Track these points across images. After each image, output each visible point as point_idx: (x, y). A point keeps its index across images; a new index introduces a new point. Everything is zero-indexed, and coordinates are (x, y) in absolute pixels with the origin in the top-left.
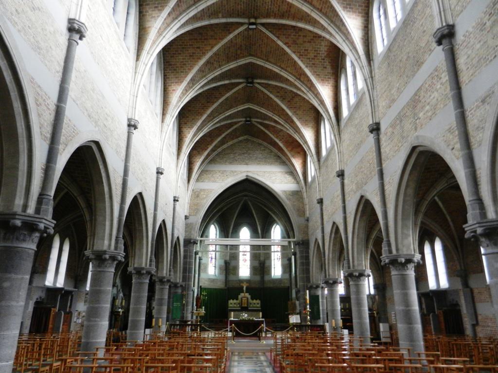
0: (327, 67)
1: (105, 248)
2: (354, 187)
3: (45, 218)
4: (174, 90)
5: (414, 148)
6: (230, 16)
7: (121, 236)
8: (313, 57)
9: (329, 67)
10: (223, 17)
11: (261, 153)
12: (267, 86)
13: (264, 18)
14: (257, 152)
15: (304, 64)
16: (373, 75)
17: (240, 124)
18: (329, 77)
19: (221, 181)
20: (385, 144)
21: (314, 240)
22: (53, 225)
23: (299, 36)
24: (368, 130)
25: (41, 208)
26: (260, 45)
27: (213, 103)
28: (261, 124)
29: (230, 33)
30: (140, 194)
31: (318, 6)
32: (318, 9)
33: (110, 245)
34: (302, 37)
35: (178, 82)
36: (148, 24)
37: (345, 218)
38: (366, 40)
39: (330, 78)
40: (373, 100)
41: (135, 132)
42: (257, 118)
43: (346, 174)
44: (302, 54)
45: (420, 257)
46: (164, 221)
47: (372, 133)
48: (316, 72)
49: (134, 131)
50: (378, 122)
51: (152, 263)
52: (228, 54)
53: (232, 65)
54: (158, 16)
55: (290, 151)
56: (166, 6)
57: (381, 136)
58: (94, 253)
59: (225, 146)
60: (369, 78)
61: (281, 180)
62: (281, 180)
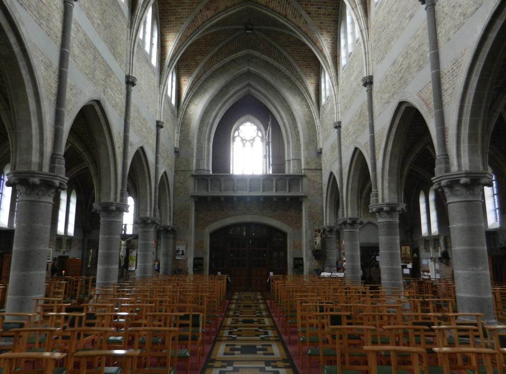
3: (60, 176)
5: (401, 104)
7: (126, 190)
16: (369, 26)
22: (66, 181)
24: (362, 83)
30: (142, 148)
33: (151, 214)
37: (373, 139)
38: (334, 49)
41: (133, 89)
43: (343, 125)
45: (405, 206)
46: (165, 173)
47: (365, 86)
49: (133, 88)
51: (157, 213)
58: (100, 204)
60: (365, 29)
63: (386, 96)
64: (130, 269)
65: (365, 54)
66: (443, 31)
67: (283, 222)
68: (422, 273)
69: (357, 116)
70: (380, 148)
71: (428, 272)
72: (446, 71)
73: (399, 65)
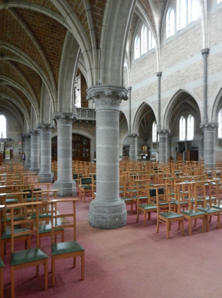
63: (171, 84)
64: (6, 158)
65: (159, 61)
66: (211, 69)
67: (90, 134)
68: (151, 158)
69: (147, 87)
70: (164, 106)
71: (155, 157)
72: (210, 85)
73: (182, 74)
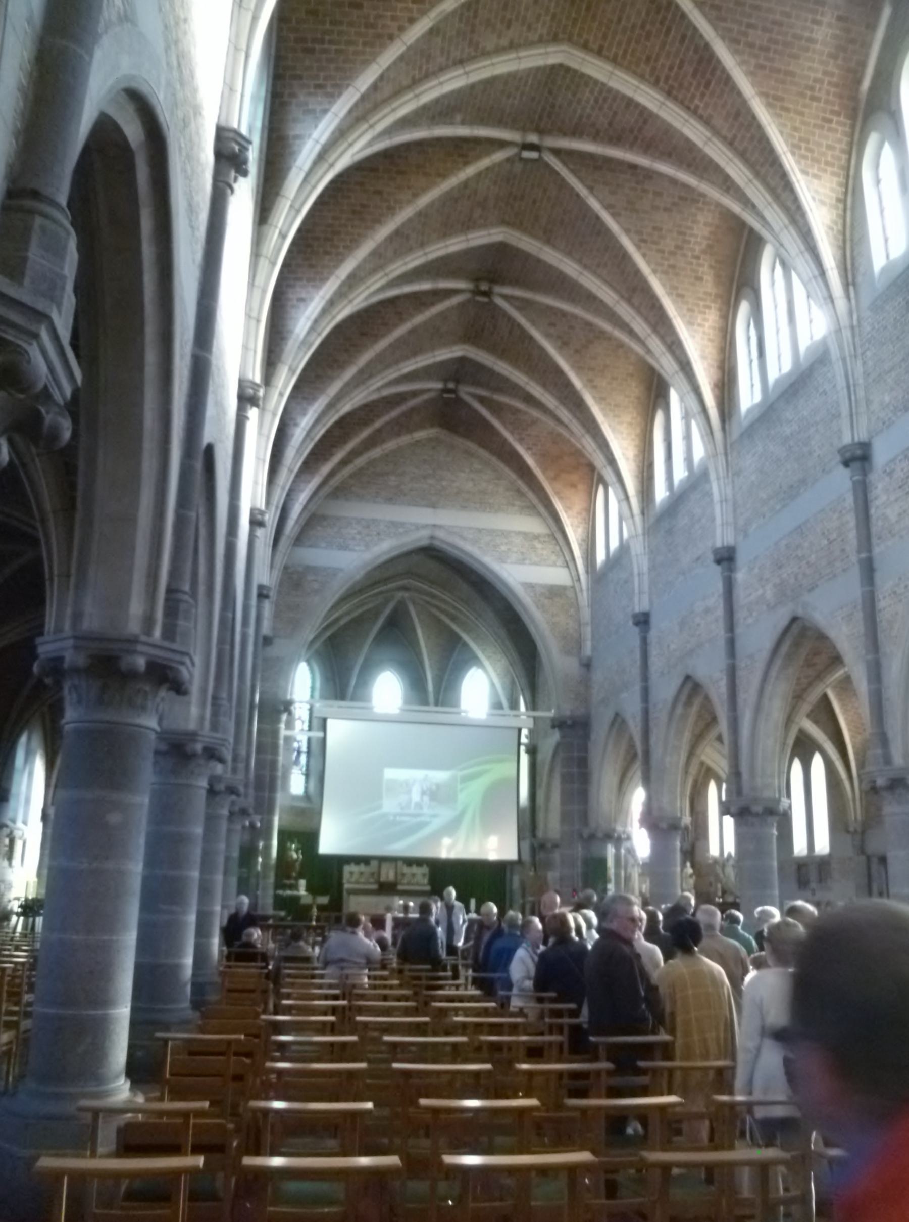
0: (705, 277)
1: (192, 726)
2: (769, 593)
4: (302, 300)
6: (483, 121)
8: (672, 249)
9: (709, 278)
10: (463, 123)
11: (472, 480)
12: (524, 305)
13: (565, 134)
14: (463, 475)
15: (649, 263)
17: (426, 397)
18: (708, 303)
19: (363, 548)
20: (884, 498)
21: (609, 715)
23: (645, 191)
25: (175, 625)
26: (534, 202)
27: (376, 338)
28: (482, 400)
29: (466, 163)
31: (724, 132)
32: (724, 139)
34: (651, 196)
35: (314, 280)
36: (295, 130)
39: (709, 307)
40: (855, 385)
42: (477, 383)
43: (742, 559)
44: (645, 237)
48: (676, 288)
50: (866, 440)
52: (451, 216)
53: (455, 245)
54: (325, 111)
55: (553, 479)
56: (348, 86)
57: (873, 477)
59: (375, 453)
61: (522, 553)
62: (522, 553)
